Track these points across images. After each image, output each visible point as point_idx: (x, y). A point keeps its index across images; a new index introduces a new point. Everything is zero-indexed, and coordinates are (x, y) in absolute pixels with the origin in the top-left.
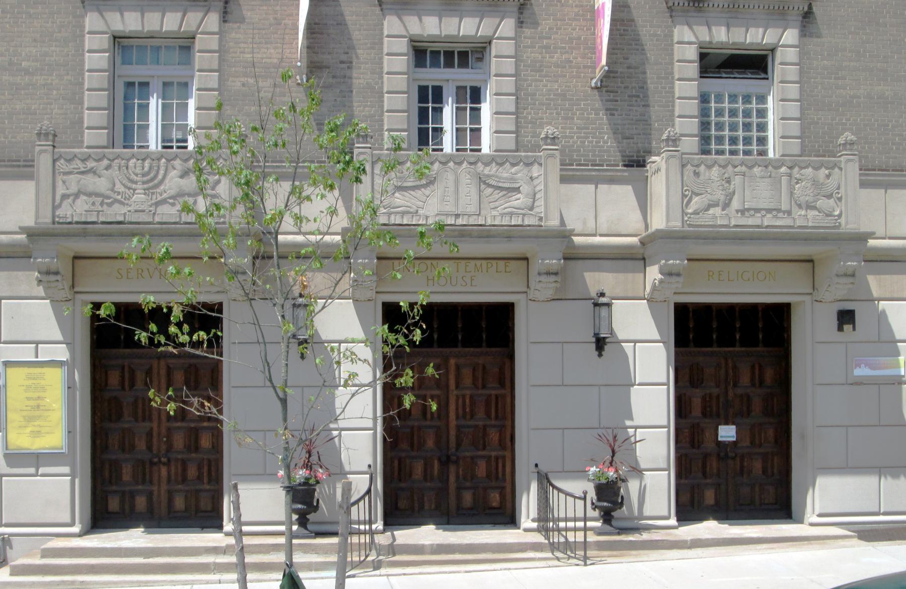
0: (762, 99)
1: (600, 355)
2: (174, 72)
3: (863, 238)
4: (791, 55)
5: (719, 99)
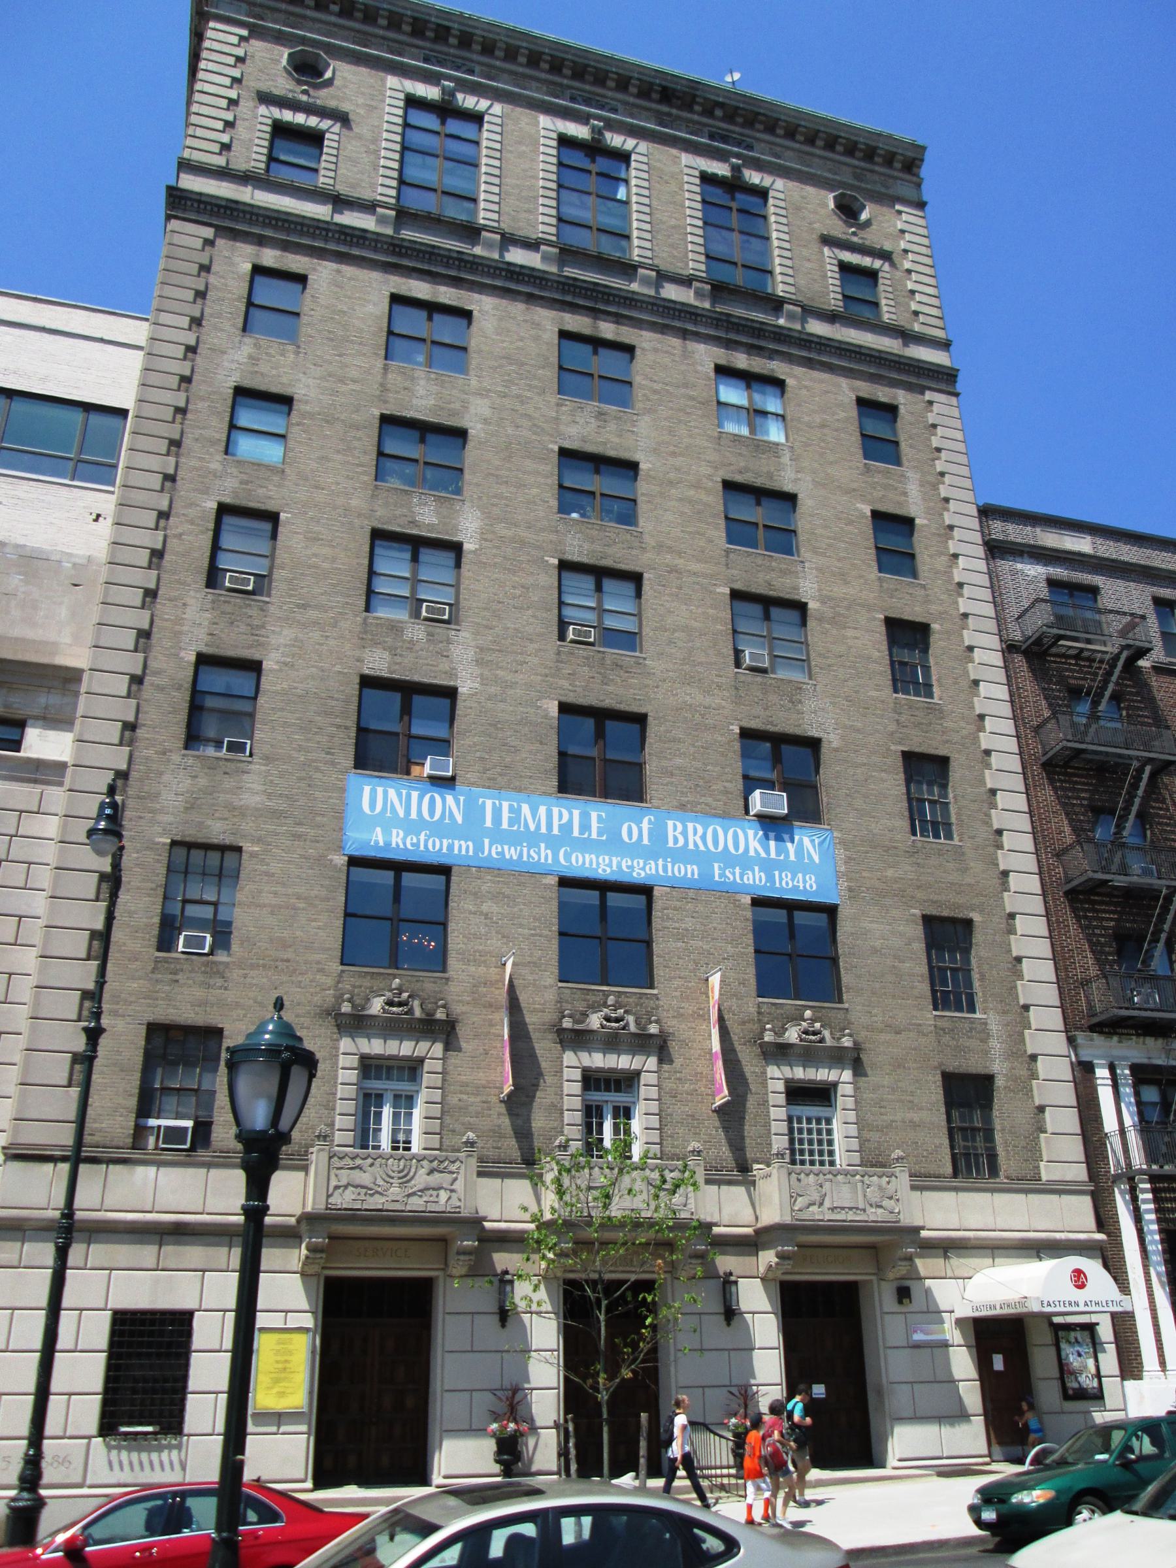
0: (829, 1121)
1: (503, 1326)
2: (404, 1087)
3: (916, 1230)
4: (651, 1078)
5: (799, 1121)
